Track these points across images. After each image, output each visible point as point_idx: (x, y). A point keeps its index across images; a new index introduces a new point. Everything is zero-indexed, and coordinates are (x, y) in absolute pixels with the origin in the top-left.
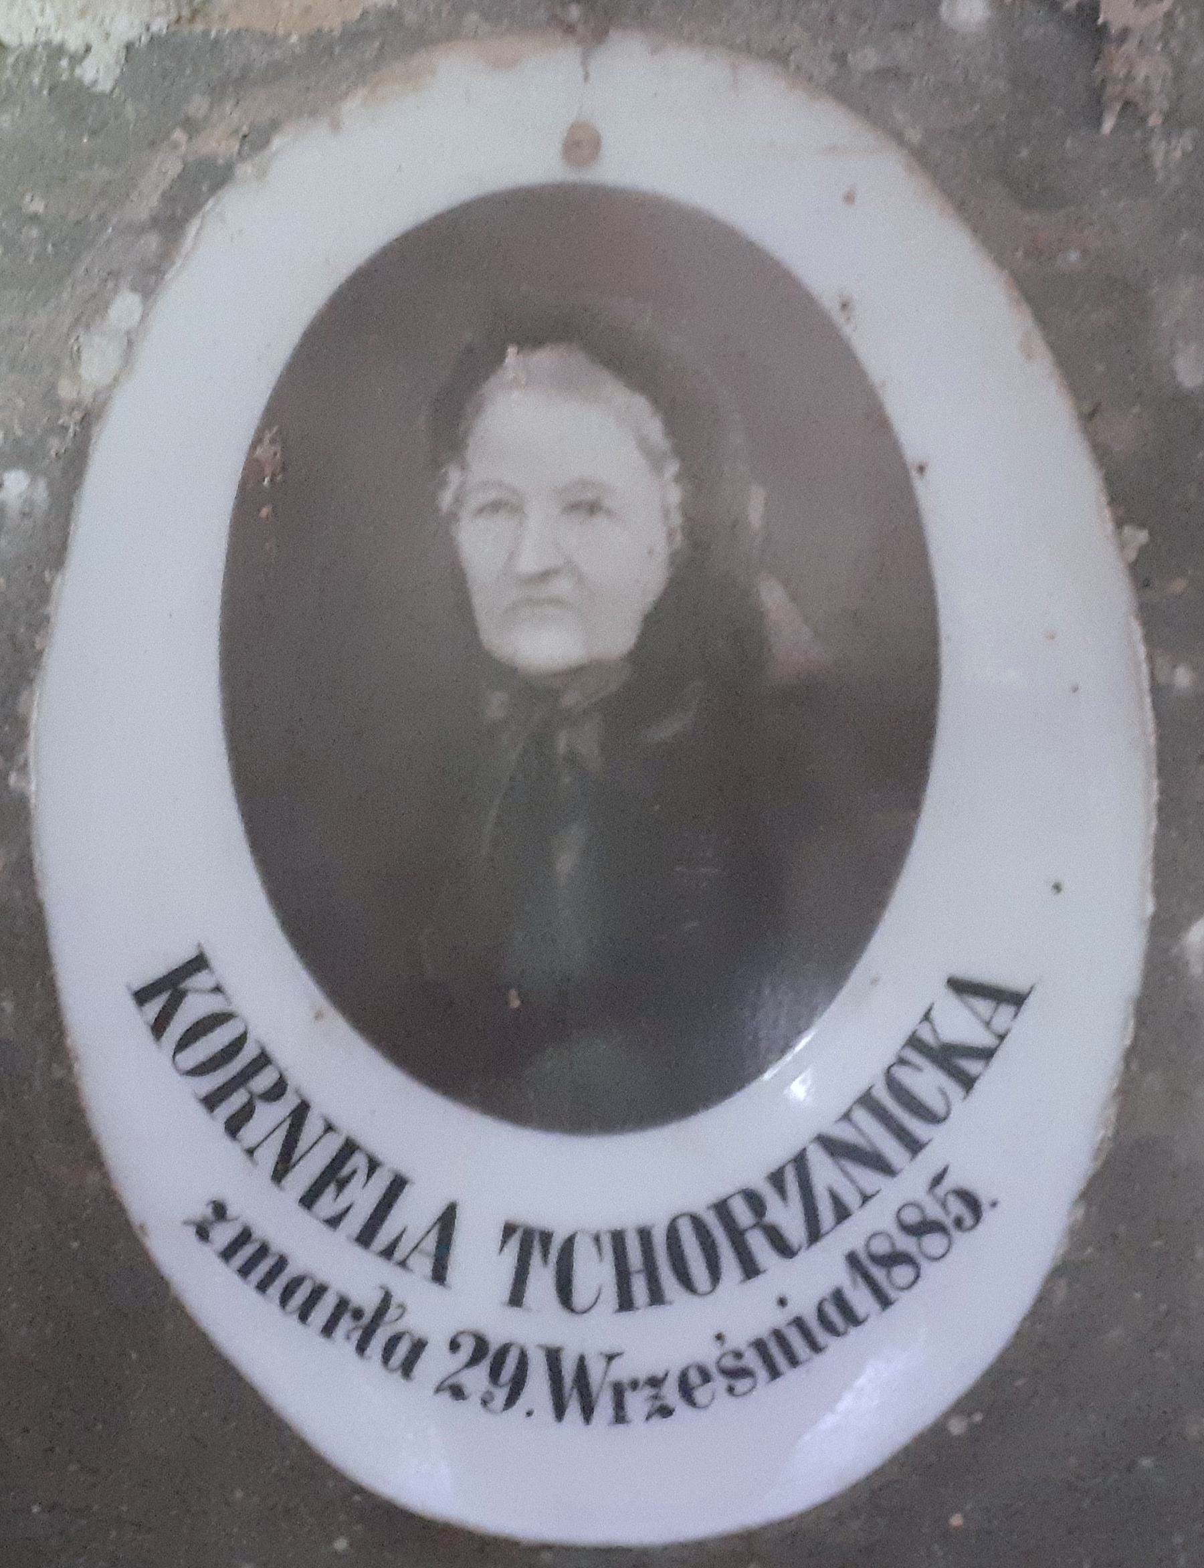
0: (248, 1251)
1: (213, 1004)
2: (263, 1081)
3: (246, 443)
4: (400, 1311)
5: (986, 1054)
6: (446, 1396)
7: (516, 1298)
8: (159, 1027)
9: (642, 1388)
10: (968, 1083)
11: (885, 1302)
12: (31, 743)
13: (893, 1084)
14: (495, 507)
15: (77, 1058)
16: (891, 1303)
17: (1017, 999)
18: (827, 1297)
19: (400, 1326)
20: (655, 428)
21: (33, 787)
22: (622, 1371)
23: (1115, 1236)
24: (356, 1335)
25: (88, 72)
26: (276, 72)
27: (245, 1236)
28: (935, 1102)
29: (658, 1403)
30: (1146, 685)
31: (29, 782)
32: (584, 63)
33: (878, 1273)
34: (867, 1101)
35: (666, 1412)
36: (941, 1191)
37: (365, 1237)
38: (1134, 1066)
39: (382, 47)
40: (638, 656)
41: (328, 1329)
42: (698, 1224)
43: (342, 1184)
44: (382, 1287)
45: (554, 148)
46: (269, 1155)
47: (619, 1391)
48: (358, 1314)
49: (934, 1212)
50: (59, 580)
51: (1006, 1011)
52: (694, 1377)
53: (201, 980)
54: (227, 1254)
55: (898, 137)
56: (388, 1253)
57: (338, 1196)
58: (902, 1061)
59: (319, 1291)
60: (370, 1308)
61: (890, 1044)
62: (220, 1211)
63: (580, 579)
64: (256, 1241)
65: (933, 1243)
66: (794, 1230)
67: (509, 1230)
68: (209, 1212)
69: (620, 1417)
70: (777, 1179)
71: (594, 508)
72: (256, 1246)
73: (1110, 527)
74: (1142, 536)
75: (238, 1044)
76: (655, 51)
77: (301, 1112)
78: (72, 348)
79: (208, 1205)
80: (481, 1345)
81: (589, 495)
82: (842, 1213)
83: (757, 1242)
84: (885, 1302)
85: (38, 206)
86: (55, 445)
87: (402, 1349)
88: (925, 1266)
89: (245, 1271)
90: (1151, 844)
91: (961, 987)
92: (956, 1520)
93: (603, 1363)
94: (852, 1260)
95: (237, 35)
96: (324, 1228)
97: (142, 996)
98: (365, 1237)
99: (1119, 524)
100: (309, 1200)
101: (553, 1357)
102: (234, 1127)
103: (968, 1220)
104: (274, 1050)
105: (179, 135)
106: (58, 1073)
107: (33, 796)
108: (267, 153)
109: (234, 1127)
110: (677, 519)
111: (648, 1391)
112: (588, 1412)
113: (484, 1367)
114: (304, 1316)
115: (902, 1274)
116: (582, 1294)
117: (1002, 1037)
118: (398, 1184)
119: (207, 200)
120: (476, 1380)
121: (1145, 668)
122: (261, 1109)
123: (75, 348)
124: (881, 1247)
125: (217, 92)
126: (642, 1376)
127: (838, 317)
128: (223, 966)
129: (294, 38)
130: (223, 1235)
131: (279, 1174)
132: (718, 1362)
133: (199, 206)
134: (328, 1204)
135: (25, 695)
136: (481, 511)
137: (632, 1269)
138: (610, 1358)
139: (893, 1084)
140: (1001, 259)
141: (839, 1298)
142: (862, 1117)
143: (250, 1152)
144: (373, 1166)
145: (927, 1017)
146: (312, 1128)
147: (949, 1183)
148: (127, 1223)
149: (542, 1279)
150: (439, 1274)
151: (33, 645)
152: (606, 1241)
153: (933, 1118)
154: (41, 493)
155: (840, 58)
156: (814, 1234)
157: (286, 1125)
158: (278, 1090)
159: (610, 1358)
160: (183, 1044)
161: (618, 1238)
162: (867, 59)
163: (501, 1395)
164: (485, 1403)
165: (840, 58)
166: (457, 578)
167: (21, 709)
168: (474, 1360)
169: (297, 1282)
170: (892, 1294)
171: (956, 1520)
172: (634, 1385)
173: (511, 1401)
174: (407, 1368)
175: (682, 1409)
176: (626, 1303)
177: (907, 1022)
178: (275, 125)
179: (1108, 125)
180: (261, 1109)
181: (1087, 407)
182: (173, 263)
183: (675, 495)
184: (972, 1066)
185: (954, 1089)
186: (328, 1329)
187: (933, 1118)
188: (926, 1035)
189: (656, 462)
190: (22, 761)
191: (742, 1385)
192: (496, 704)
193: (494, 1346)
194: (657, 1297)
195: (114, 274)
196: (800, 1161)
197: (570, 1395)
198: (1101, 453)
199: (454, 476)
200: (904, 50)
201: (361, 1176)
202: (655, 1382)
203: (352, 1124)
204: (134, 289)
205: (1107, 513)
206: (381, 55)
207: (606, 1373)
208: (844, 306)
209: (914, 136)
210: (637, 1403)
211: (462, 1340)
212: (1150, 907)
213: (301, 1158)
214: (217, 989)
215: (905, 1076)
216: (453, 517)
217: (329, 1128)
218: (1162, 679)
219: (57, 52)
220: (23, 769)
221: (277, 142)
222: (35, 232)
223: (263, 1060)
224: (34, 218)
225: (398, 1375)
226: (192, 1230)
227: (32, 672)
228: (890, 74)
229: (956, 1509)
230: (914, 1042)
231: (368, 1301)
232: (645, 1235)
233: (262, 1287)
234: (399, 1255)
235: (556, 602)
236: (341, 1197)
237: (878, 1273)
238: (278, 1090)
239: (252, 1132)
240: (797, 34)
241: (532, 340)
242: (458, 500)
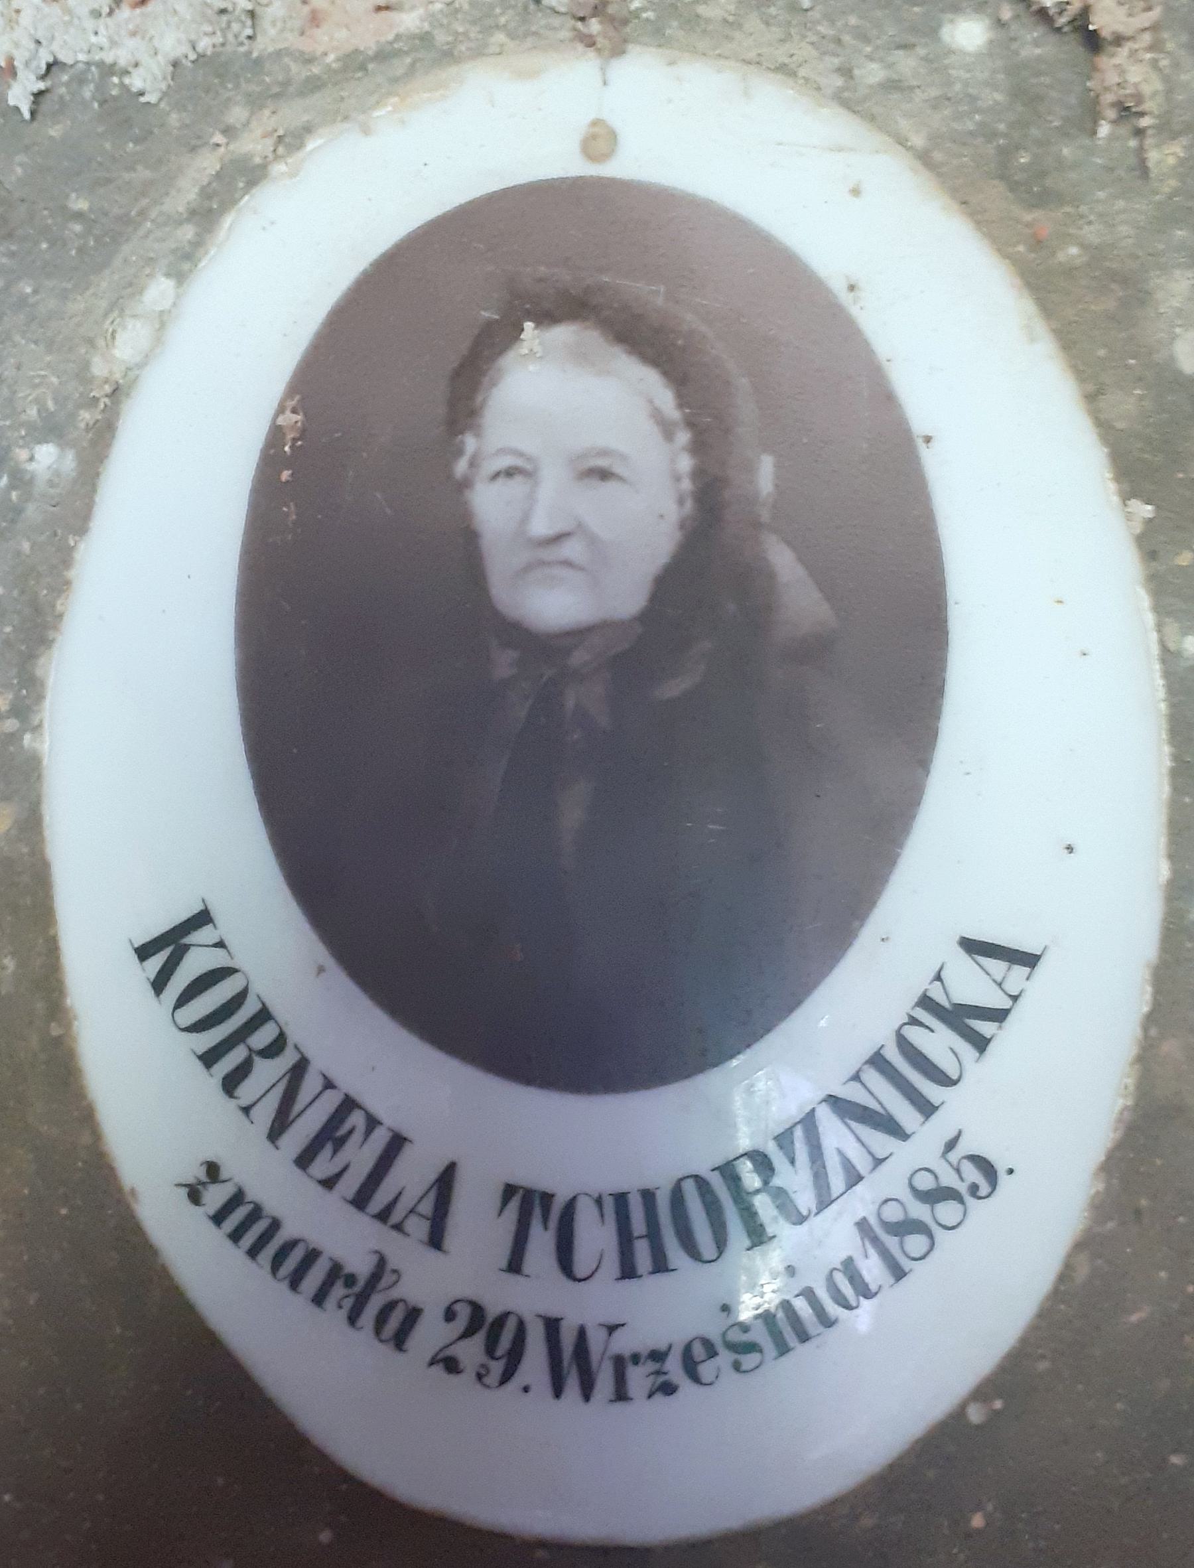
1: (217, 959)
2: (263, 1037)
3: (271, 412)
4: (394, 1277)
5: (998, 1016)
6: (438, 1371)
7: (515, 1265)
8: (159, 984)
9: (644, 1364)
10: (981, 1044)
12: (47, 703)
13: (903, 1044)
14: (510, 473)
15: (75, 1018)
16: (905, 1274)
17: (1030, 960)
18: (839, 1266)
19: (395, 1294)
20: (666, 399)
21: (46, 746)
22: (623, 1343)
23: (1138, 1213)
24: (348, 1303)
25: (136, 82)
26: (313, 85)
27: (237, 1199)
28: (947, 1065)
29: (662, 1379)
30: (1155, 650)
31: (42, 742)
32: (603, 70)
33: (891, 1242)
34: (877, 1061)
35: (668, 1389)
36: (954, 1156)
37: (360, 1201)
38: (1153, 1032)
39: (413, 65)
40: (647, 617)
41: (319, 1299)
43: (340, 1143)
44: (377, 1252)
45: (572, 145)
46: (266, 1113)
47: (620, 1363)
48: (350, 1280)
49: (948, 1179)
50: (82, 546)
51: (1020, 971)
52: (698, 1351)
53: (204, 935)
54: (218, 1218)
55: (901, 141)
56: (383, 1216)
57: (332, 1157)
58: (914, 1021)
59: (312, 1256)
61: (902, 1005)
62: (213, 1170)
63: (593, 541)
65: (947, 1211)
66: (805, 1199)
67: (510, 1191)
68: (202, 1174)
69: (621, 1395)
70: (784, 1139)
71: (604, 475)
72: (250, 1207)
73: (1116, 499)
74: (1148, 510)
75: (239, 999)
76: (672, 63)
77: (300, 1069)
78: (107, 330)
79: (201, 1165)
80: (477, 1310)
81: (602, 462)
82: (854, 1178)
83: (763, 1205)
84: (899, 1274)
85: (81, 205)
86: (86, 416)
87: (395, 1320)
88: (939, 1233)
89: (235, 1236)
90: (1165, 810)
91: (974, 947)
92: (977, 1521)
93: (603, 1333)
94: (863, 1226)
95: (279, 54)
96: (320, 1189)
97: (144, 952)
98: (360, 1201)
99: (1126, 497)
100: (304, 1160)
101: (552, 1326)
102: (230, 1084)
103: (984, 1189)
104: (275, 1008)
105: (219, 138)
106: (55, 1031)
107: (47, 756)
108: (301, 154)
109: (230, 1084)
110: (687, 485)
111: (651, 1366)
112: (587, 1392)
113: (479, 1339)
114: (295, 1282)
115: (916, 1244)
116: (583, 1260)
117: (1015, 998)
118: (397, 1142)
119: (242, 197)
120: (471, 1352)
121: (1154, 636)
122: (260, 1064)
123: (111, 330)
124: (893, 1213)
125: (256, 103)
126: (644, 1351)
127: (844, 297)
128: (226, 925)
129: (331, 57)
130: (216, 1196)
131: (276, 1131)
132: (724, 1334)
133: (235, 202)
134: (323, 1165)
135: (42, 661)
136: (496, 476)
137: (636, 1234)
138: (612, 1329)
139: (903, 1044)
140: (1002, 248)
142: (873, 1078)
143: (246, 1110)
144: (373, 1123)
145: (938, 978)
146: (311, 1085)
147: (963, 1148)
148: (120, 1189)
149: (542, 1242)
150: (436, 1240)
151: (53, 606)
152: (609, 1205)
153: (945, 1081)
154: (69, 462)
155: (846, 72)
157: (285, 1081)
158: (276, 1048)
159: (612, 1329)
160: (184, 999)
161: (621, 1199)
162: (872, 73)
163: (497, 1368)
164: (480, 1377)
165: (846, 72)
166: (469, 537)
167: (39, 672)
168: (468, 1333)
170: (906, 1264)
171: (977, 1521)
172: (636, 1359)
173: (506, 1377)
174: (400, 1341)
175: (687, 1387)
176: (628, 1271)
177: (920, 983)
178: (308, 129)
179: (1104, 130)
180: (260, 1064)
181: (1091, 388)
182: (206, 253)
183: (686, 463)
184: (985, 1028)
185: (966, 1050)
187: (945, 1081)
188: (937, 994)
189: (667, 430)
190: (36, 722)
191: (749, 1360)
192: (504, 663)
193: (492, 1312)
194: (661, 1266)
195: (151, 261)
196: (809, 1121)
197: (569, 1372)
198: (1105, 429)
199: (470, 443)
200: (907, 64)
201: (357, 1136)
202: (658, 1356)
203: (349, 1083)
204: (168, 275)
205: (1112, 486)
206: (411, 71)
207: (607, 1343)
208: (852, 288)
209: (918, 141)
210: (638, 1379)
211: (458, 1307)
212: (1164, 871)
213: (299, 1115)
214: (220, 944)
215: (915, 1035)
216: (465, 484)
217: (329, 1085)
218: (1172, 646)
219: (109, 70)
220: (37, 729)
221: (311, 145)
222: (78, 228)
223: (263, 1016)
224: (79, 216)
226: (184, 1192)
227: (51, 634)
228: (893, 86)
229: (979, 1507)
230: (926, 1002)
231: (360, 1265)
232: (648, 1196)
233: (253, 1253)
234: (395, 1217)
235: (568, 563)
236: (336, 1159)
237: (891, 1242)
238: (276, 1048)
239: (248, 1090)
240: (804, 51)
241: (546, 317)
242: (473, 464)
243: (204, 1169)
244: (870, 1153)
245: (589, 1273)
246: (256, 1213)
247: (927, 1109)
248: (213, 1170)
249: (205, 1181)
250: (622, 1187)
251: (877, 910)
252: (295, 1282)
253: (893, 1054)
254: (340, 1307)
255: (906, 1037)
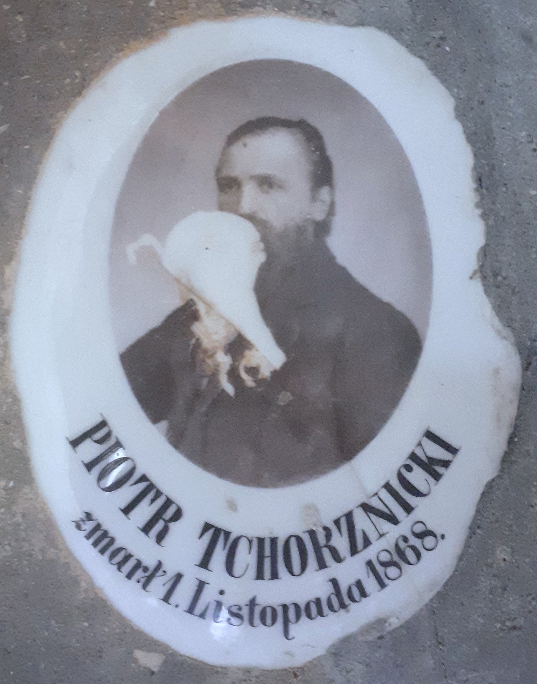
0: (99, 533)
10: (437, 477)
11: (383, 585)
24: (143, 580)
33: (380, 569)
41: (129, 576)
42: (299, 540)
48: (146, 569)
59: (128, 557)
60: (151, 569)
61: (401, 458)
62: (89, 516)
64: (110, 537)
67: (207, 527)
68: (83, 516)
70: (337, 522)
82: (367, 542)
83: (326, 554)
84: (383, 585)
94: (369, 563)
114: (120, 566)
115: (392, 571)
130: (89, 526)
141: (359, 584)
156: (354, 551)
161: (261, 541)
169: (119, 550)
170: (386, 581)
176: (260, 576)
186: (129, 576)
196: (349, 516)
225: (115, 567)
230: (413, 457)
243: (85, 514)
244: (379, 533)
245: (241, 573)
246: (105, 534)
247: (408, 509)
248: (89, 516)
249: (85, 520)
250: (261, 535)
251: (453, 463)
252: (120, 566)
253: (396, 484)
254: (138, 582)
255: (412, 484)
